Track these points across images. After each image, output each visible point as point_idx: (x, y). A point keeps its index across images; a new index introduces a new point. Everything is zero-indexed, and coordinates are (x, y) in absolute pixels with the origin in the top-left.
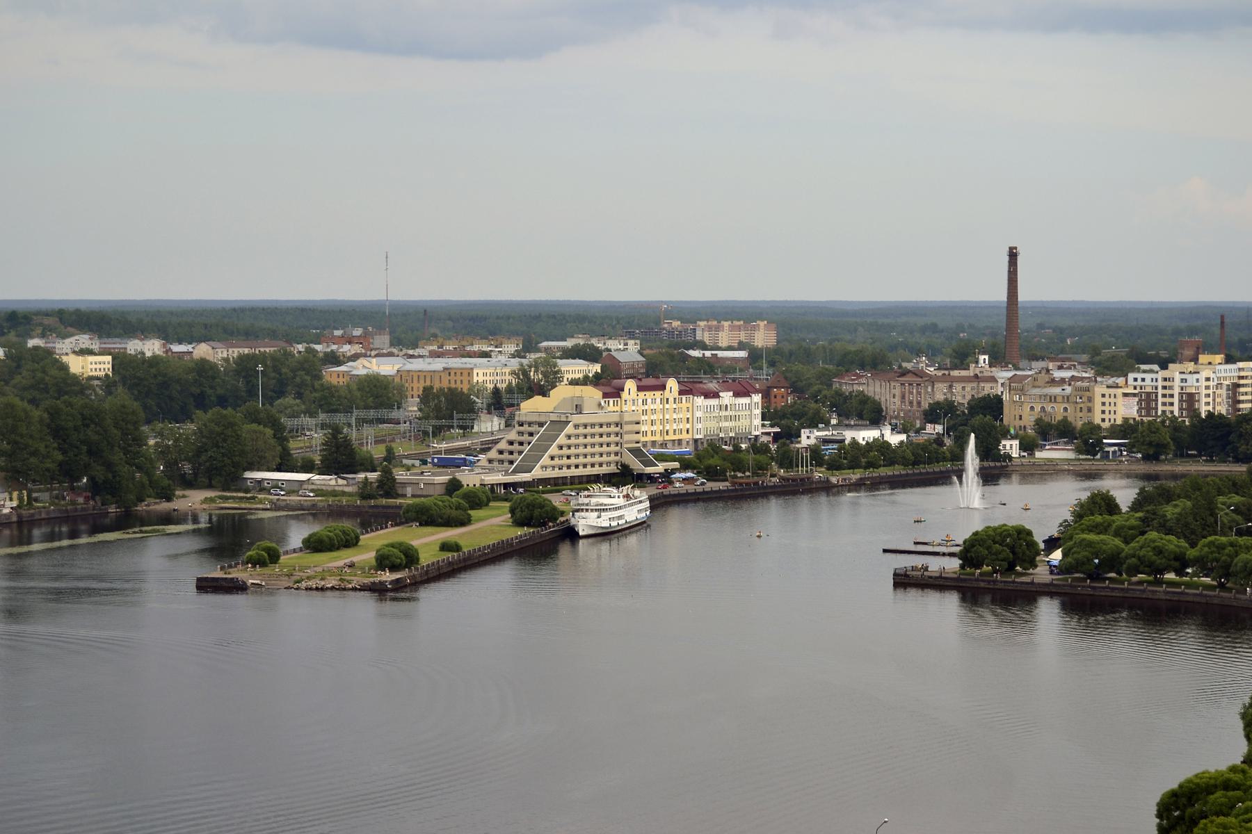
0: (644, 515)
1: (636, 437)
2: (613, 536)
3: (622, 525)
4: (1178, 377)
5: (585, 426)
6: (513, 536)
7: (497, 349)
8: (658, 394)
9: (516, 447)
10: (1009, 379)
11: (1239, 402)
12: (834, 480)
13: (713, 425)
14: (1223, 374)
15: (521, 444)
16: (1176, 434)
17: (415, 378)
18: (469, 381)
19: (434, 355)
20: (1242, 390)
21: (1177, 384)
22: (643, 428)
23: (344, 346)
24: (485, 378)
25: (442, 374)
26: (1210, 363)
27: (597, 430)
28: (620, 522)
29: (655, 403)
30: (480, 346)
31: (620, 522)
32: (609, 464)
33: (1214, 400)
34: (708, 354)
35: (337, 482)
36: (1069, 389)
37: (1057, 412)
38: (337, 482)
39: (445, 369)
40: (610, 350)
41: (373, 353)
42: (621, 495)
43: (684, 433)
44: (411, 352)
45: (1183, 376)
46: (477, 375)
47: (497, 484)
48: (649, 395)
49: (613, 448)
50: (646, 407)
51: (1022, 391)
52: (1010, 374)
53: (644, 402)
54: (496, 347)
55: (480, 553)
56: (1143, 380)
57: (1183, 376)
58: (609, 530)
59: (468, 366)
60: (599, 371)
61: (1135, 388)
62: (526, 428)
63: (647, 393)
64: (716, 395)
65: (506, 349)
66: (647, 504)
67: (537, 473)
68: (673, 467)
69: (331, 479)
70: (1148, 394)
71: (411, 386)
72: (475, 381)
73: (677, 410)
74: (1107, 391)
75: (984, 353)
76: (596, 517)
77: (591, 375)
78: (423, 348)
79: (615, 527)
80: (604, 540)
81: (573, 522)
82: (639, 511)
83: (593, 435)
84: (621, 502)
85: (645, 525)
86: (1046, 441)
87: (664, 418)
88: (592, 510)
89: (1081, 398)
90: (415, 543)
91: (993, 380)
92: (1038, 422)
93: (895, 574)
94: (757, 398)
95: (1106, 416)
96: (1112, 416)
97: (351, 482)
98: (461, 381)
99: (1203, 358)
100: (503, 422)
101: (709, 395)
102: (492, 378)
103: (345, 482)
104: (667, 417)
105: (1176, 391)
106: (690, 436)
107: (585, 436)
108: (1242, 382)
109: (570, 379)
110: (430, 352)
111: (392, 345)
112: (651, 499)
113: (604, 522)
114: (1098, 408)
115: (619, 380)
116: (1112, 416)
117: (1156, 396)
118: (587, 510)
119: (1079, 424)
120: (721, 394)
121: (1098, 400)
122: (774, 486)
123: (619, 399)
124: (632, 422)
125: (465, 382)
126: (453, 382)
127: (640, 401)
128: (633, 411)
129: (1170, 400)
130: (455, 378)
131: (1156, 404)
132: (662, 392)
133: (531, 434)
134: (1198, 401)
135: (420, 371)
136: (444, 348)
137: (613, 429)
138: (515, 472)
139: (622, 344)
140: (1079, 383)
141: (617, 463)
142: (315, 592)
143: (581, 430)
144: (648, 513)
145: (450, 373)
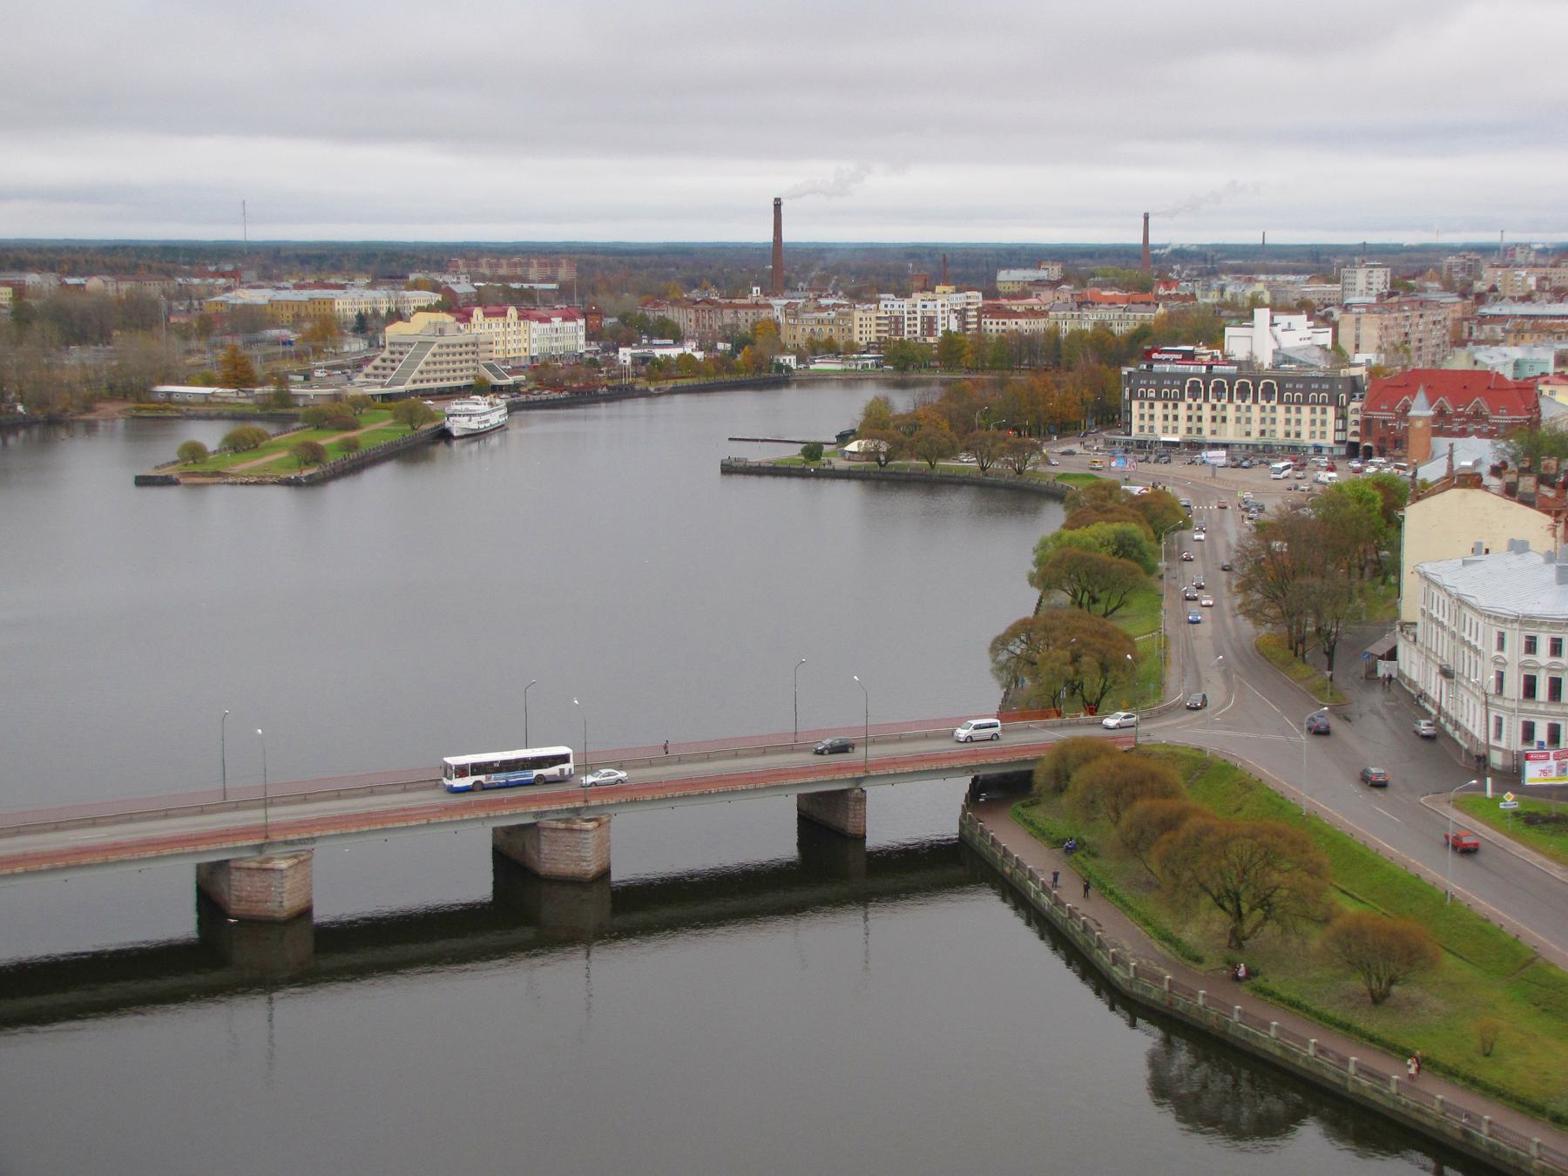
0: (503, 419)
1: (489, 355)
2: (480, 436)
4: (920, 304)
5: (448, 346)
8: (501, 319)
9: (388, 364)
10: (785, 306)
11: (968, 323)
12: (652, 389)
13: (547, 344)
14: (955, 301)
19: (298, 287)
20: (969, 313)
21: (919, 309)
22: (495, 348)
26: (944, 292)
27: (458, 349)
28: (487, 425)
31: (487, 425)
32: (467, 377)
33: (948, 322)
34: (526, 286)
36: (833, 314)
37: (825, 332)
39: (310, 299)
40: (447, 283)
41: (245, 286)
43: (523, 350)
44: (278, 284)
45: (924, 303)
48: (494, 320)
49: (471, 364)
51: (796, 315)
52: (785, 302)
53: (490, 326)
54: (350, 280)
56: (893, 306)
57: (924, 303)
59: (331, 297)
60: (440, 299)
61: (886, 313)
62: (396, 348)
64: (547, 320)
66: (504, 411)
67: (408, 386)
70: (897, 318)
72: (336, 309)
74: (863, 316)
75: (756, 285)
80: (475, 441)
81: (448, 425)
83: (454, 354)
84: (486, 408)
85: (504, 428)
86: (816, 355)
88: (464, 416)
89: (843, 321)
91: (770, 306)
92: (810, 340)
93: (722, 465)
94: (582, 322)
95: (863, 336)
96: (868, 336)
97: (249, 394)
99: (939, 289)
101: (542, 320)
102: (351, 307)
103: (245, 395)
105: (919, 316)
106: (527, 354)
107: (448, 355)
108: (969, 307)
111: (260, 278)
113: (474, 425)
114: (857, 329)
116: (868, 336)
117: (903, 319)
118: (460, 415)
119: (842, 343)
120: (552, 319)
121: (857, 323)
122: (605, 395)
127: (486, 325)
129: (910, 322)
131: (903, 326)
133: (401, 353)
134: (936, 323)
137: (471, 348)
138: (390, 385)
140: (841, 309)
143: (445, 350)
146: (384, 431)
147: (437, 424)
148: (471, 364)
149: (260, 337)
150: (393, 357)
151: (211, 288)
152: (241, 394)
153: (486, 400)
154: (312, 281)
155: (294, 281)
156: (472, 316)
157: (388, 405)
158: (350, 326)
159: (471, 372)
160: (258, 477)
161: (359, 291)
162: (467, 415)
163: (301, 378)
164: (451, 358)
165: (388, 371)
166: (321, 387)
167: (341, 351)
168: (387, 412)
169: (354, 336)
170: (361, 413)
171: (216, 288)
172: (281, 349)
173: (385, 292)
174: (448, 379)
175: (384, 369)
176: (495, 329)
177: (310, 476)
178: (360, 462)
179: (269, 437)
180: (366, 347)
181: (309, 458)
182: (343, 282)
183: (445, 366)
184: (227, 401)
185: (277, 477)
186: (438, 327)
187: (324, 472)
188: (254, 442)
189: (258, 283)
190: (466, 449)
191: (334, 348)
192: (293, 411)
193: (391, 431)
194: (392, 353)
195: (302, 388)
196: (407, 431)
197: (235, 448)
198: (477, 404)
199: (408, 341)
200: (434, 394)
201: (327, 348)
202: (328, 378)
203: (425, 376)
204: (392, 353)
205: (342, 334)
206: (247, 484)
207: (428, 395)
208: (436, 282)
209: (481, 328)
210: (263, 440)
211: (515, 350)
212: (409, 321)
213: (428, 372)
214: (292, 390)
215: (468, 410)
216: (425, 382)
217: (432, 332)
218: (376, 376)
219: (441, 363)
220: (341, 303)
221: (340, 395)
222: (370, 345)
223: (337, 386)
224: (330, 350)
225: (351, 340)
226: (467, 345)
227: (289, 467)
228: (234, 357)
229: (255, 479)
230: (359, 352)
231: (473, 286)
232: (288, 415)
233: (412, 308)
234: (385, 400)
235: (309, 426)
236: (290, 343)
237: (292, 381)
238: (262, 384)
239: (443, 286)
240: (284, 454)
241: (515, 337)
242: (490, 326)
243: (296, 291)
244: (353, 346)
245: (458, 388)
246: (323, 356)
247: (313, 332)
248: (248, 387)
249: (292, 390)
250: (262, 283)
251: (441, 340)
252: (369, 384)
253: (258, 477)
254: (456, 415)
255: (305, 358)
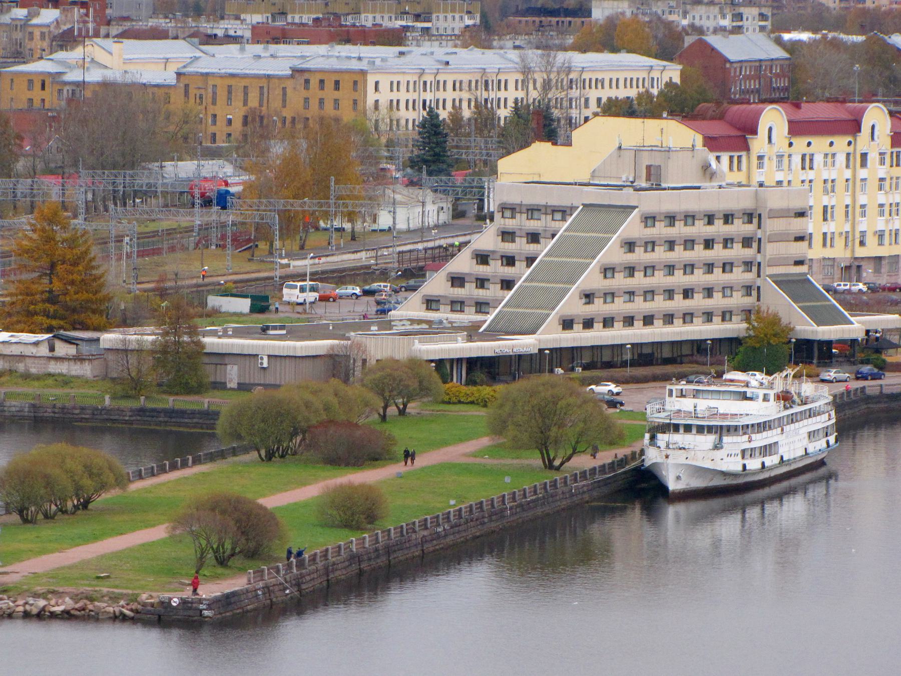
0: (821, 444)
1: (797, 250)
3: (771, 468)
5: (671, 219)
6: (473, 503)
7: (420, 25)
8: (841, 142)
9: (496, 269)
15: (510, 261)
16: (74, 251)
17: (222, 95)
18: (355, 102)
22: (813, 225)
23: (44, 11)
24: (395, 96)
25: (289, 84)
27: (700, 229)
29: (833, 164)
30: (378, 16)
32: (726, 315)
35: (52, 349)
38: (52, 349)
39: (297, 71)
40: (700, 31)
41: (115, 30)
42: (772, 393)
46: (376, 89)
47: (452, 361)
48: (820, 144)
49: (739, 276)
50: (811, 175)
53: (807, 162)
54: (417, 17)
55: (426, 533)
58: (741, 481)
59: (355, 65)
60: (677, 80)
63: (814, 140)
65: (441, 24)
66: (826, 420)
68: (885, 327)
69: (36, 344)
71: (211, 112)
72: (370, 101)
73: (887, 184)
76: (711, 446)
77: (655, 91)
78: (237, 18)
79: (755, 473)
80: (727, 510)
81: (652, 456)
82: (812, 435)
83: (689, 243)
84: (771, 410)
85: (822, 471)
87: (854, 201)
88: (700, 429)
90: (271, 502)
97: (85, 349)
98: (336, 101)
100: (447, 205)
102: (411, 96)
103: (71, 350)
104: (862, 199)
109: (604, 100)
110: (254, 28)
112: (840, 404)
115: (744, 106)
118: (688, 428)
123: (744, 154)
124: (788, 210)
125: (346, 105)
126: (314, 104)
127: (797, 160)
128: (780, 183)
130: (321, 94)
132: (850, 138)
133: (534, 238)
135: (233, 76)
136: (289, 20)
137: (739, 228)
138: (493, 333)
139: (729, 17)
141: (748, 312)
142: (19, 623)
143: (661, 230)
144: (832, 439)
145: (307, 82)
146: (466, 469)
147: (622, 452)
148: (739, 276)
149: (142, 180)
150: (509, 248)
151: (18, 35)
152: (62, 349)
153: (771, 386)
154: (308, 18)
155: (257, 18)
156: (754, 132)
157: (486, 391)
158: (404, 153)
159: (738, 300)
160: (76, 598)
161: (440, 51)
162: (710, 429)
163: (243, 305)
164: (680, 254)
165: (493, 291)
166: (293, 334)
167: (369, 226)
168: (480, 412)
169: (411, 183)
170: (402, 412)
171: (31, 35)
172: (198, 217)
173: (514, 55)
174: (669, 319)
175: (481, 283)
176: (821, 172)
177: (228, 600)
178: (382, 561)
179: (122, 481)
180: (444, 217)
181: (228, 546)
182: (399, 23)
183: (659, 279)
184: (21, 367)
185: (134, 598)
186: (646, 160)
187: (267, 589)
188: (78, 489)
189: (152, 23)
190: (702, 537)
191: (351, 217)
192: (205, 402)
193: (483, 471)
194: (507, 235)
195: (238, 333)
196: (531, 469)
197: (21, 512)
198: (744, 397)
199: (554, 202)
200: (624, 364)
201: (326, 215)
202: (320, 309)
203: (599, 308)
204: (507, 235)
205: (381, 177)
206: (42, 616)
207: (609, 365)
208: (669, 25)
209: (779, 167)
210: (103, 487)
211: (881, 235)
212: (568, 143)
213: (609, 295)
214: (207, 340)
215: (715, 415)
216: (678, 322)
217: (626, 175)
218: (457, 305)
219: (649, 269)
220: (384, 86)
221: (347, 357)
222: (458, 214)
223: (339, 331)
224: (337, 224)
225: (401, 194)
226: (728, 218)
227: (170, 571)
228: (49, 239)
229: (67, 603)
230: (422, 232)
231: (779, 42)
232: (193, 413)
233: (593, 104)
234: (479, 375)
235: (246, 450)
236: (223, 200)
237: (215, 315)
238: (125, 322)
239: (689, 40)
240: (158, 533)
241: (882, 198)
242: (807, 162)
243: (258, 48)
244: (401, 213)
245: (699, 347)
246: (314, 238)
247: (290, 168)
248: (85, 327)
249: (207, 340)
250: (161, 22)
251: (652, 202)
252: (432, 330)
253: (76, 598)
254: (676, 428)
255: (263, 246)
